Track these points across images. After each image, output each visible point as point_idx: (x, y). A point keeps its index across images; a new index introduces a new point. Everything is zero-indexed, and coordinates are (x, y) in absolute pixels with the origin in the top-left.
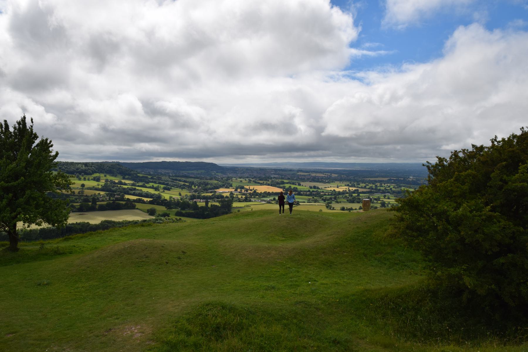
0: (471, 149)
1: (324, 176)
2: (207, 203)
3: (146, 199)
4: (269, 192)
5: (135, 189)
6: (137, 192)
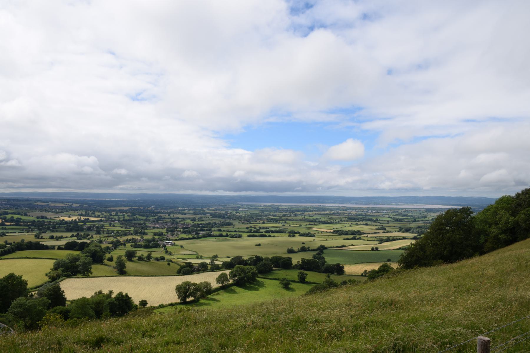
0: (124, 294)
1: (64, 205)
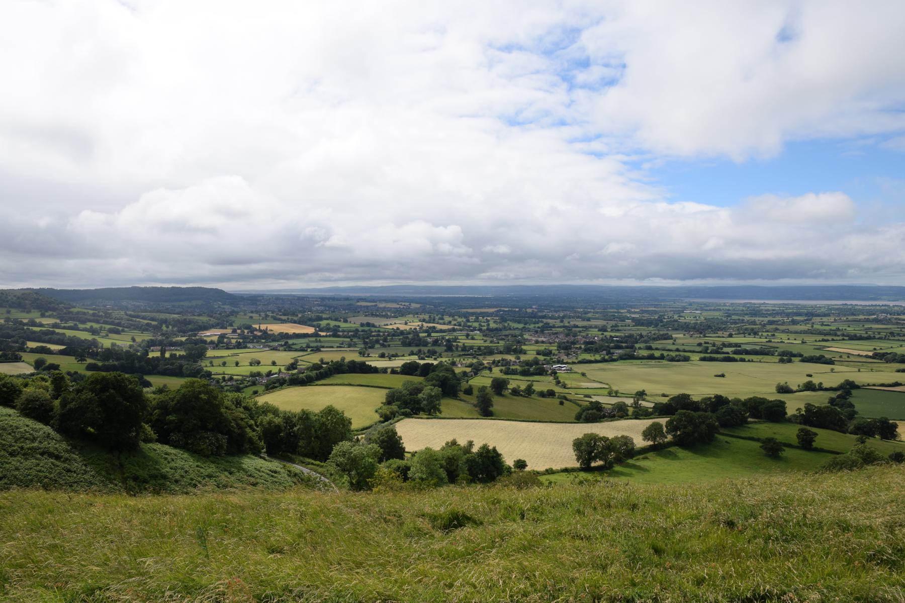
2: (163, 352)
3: (53, 347)
4: (287, 334)
5: (53, 333)
6: (55, 337)
